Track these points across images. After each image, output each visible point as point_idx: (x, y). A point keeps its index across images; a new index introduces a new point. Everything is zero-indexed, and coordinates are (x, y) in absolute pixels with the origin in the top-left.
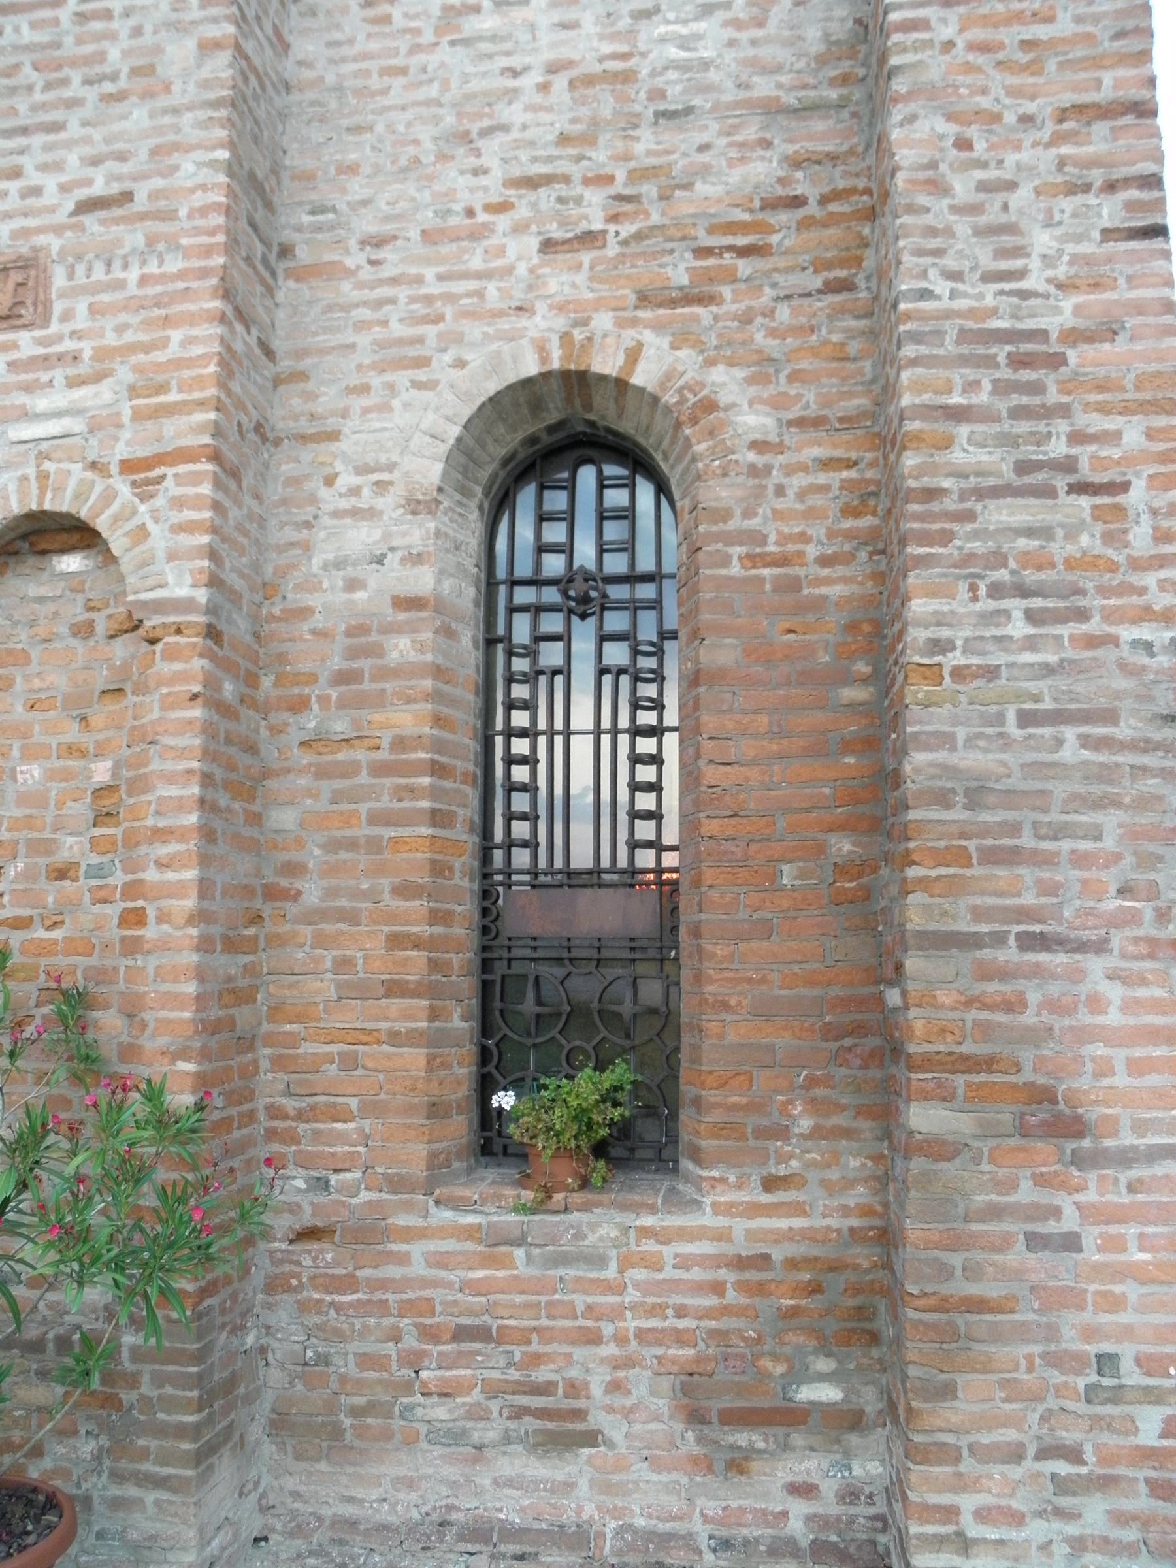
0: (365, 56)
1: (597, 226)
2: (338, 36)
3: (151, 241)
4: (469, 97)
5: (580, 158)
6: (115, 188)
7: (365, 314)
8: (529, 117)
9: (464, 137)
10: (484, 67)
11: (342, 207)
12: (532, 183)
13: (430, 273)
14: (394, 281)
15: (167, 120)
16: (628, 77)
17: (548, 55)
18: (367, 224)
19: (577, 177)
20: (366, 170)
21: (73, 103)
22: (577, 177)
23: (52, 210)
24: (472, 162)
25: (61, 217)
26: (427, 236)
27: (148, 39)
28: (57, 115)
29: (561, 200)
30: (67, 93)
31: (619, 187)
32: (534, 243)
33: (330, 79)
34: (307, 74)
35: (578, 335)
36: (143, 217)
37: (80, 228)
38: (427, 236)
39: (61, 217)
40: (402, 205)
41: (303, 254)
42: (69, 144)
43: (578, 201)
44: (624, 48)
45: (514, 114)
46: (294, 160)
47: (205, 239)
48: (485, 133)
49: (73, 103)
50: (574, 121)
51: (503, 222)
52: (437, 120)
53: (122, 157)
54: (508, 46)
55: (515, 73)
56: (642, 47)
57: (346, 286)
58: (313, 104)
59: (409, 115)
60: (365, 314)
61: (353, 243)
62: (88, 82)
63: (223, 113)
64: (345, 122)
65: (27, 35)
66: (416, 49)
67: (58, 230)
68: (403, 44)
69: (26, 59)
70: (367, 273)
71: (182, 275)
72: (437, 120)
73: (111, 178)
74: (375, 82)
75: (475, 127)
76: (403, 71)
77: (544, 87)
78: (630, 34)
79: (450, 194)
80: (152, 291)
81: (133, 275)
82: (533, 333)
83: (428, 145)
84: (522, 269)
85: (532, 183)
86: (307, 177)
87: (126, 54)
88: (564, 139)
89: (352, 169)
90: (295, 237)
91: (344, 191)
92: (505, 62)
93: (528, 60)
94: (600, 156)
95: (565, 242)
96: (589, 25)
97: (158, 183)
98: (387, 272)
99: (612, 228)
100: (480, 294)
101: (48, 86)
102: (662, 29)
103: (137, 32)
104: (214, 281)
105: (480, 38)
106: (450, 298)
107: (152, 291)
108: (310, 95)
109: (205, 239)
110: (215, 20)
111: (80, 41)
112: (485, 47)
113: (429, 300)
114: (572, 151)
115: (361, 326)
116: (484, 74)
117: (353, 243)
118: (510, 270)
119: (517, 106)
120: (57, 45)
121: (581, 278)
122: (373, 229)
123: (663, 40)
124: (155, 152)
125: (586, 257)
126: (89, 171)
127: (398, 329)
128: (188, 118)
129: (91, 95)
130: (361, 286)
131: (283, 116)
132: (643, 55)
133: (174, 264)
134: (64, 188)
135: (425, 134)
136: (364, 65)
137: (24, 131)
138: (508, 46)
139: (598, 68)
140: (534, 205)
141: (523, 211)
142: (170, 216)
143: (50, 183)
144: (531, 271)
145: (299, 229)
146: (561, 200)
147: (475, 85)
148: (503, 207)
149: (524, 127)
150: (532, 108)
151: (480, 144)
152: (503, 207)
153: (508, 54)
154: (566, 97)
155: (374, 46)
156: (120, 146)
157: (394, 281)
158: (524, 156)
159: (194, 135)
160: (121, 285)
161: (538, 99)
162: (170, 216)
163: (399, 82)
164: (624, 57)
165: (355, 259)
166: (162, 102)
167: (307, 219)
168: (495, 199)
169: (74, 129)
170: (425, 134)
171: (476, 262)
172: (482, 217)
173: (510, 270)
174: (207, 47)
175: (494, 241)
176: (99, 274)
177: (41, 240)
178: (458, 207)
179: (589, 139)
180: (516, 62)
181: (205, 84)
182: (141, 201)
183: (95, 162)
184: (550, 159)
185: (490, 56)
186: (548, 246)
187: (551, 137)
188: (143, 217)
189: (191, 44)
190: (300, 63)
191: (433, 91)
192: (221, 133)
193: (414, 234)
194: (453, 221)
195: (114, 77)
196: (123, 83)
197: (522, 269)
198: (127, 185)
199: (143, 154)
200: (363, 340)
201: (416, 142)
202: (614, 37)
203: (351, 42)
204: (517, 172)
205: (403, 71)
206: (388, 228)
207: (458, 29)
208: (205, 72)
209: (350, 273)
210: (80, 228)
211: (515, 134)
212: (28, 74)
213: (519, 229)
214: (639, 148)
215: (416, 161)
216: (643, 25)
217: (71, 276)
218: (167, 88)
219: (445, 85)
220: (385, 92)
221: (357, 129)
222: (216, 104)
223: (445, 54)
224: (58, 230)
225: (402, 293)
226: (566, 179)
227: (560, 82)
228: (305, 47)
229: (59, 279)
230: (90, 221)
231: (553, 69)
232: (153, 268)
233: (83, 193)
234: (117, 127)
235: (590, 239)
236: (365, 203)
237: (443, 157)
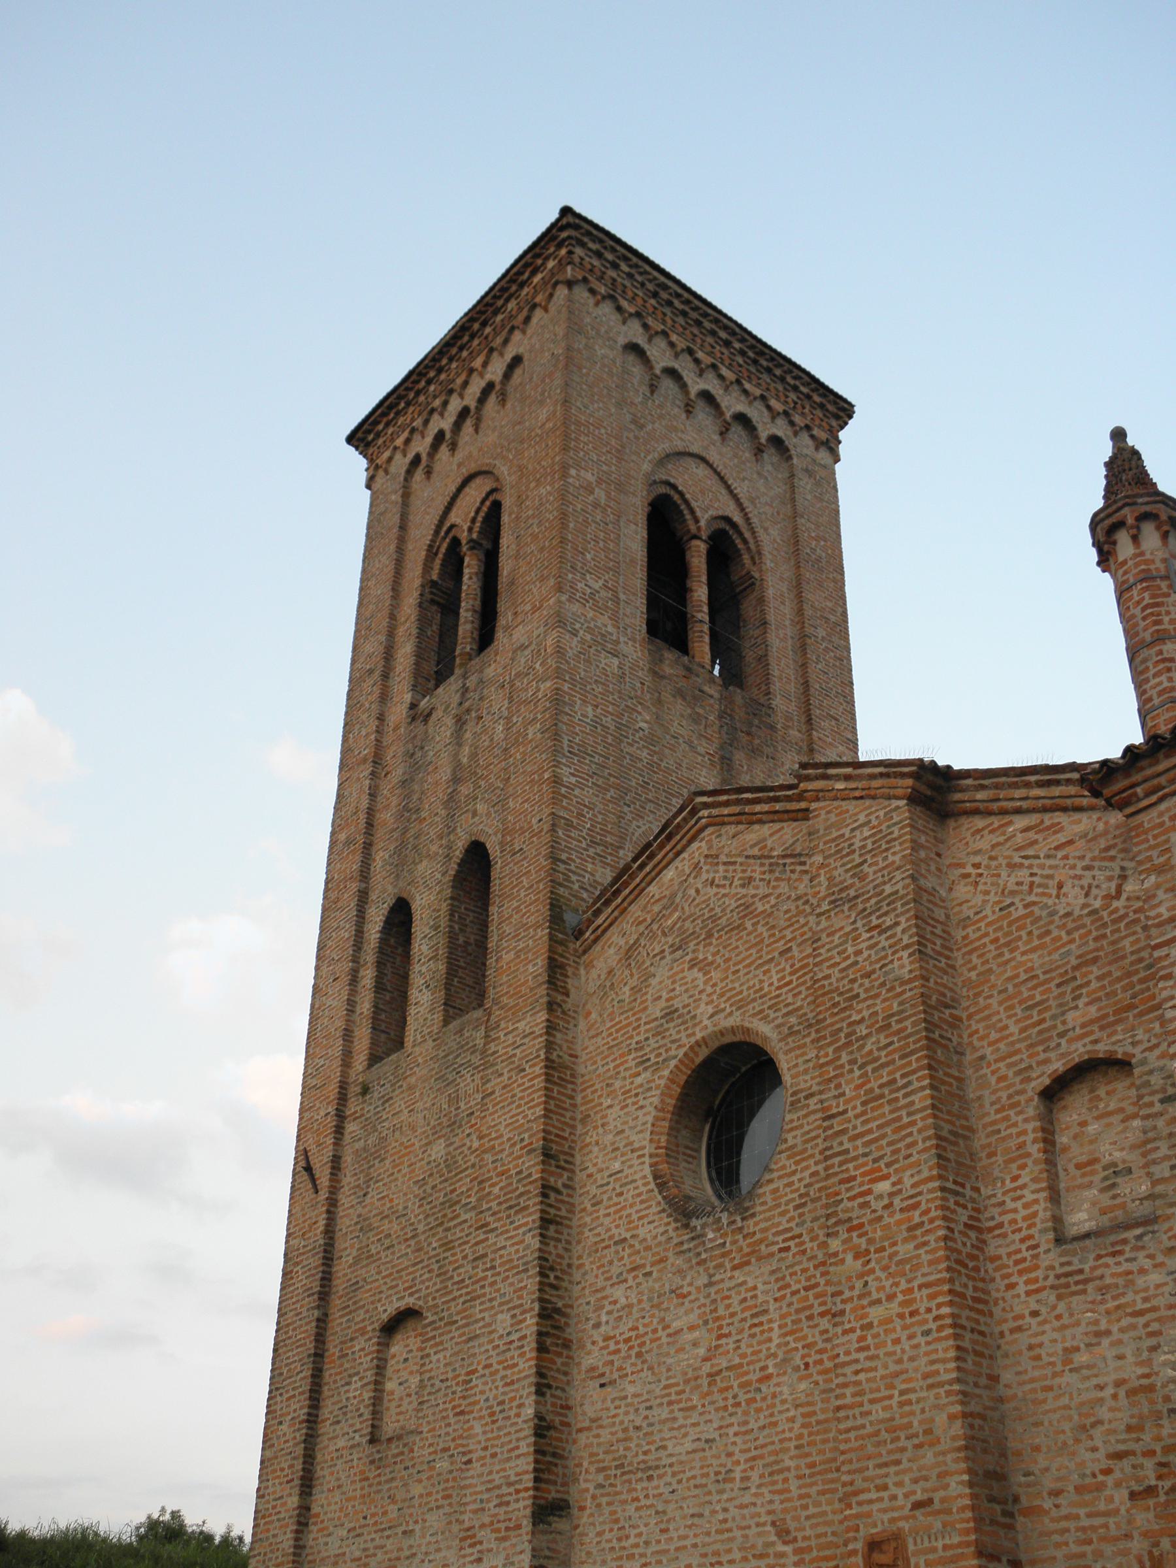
0: (1032, 1380)
1: (1153, 1483)
2: (1020, 1369)
3: (944, 1525)
4: (1082, 1404)
5: (1138, 1440)
6: (925, 1496)
7: (1056, 1538)
8: (1110, 1415)
9: (1083, 1428)
10: (1088, 1384)
11: (1037, 1472)
12: (1119, 1456)
13: (1082, 1512)
14: (1067, 1517)
15: (941, 1458)
16: (1151, 1388)
17: (1114, 1376)
18: (1048, 1483)
19: (1138, 1452)
20: (1044, 1449)
21: (903, 1450)
22: (1138, 1452)
23: (902, 1508)
24: (1090, 1444)
25: (906, 1512)
26: (1079, 1489)
27: (927, 1415)
28: (896, 1456)
29: (1134, 1467)
30: (900, 1444)
31: (1160, 1458)
32: (1125, 1493)
33: (1020, 1394)
34: (1010, 1392)
35: (1156, 1553)
36: (939, 1512)
37: (914, 1517)
38: (1079, 1489)
39: (906, 1512)
40: (1064, 1472)
41: (1025, 1502)
42: (904, 1472)
43: (1142, 1466)
44: (1146, 1370)
45: (1103, 1413)
46: (1012, 1444)
47: (965, 1525)
48: (1093, 1425)
49: (903, 1450)
50: (1132, 1417)
51: (1109, 1480)
52: (1070, 1418)
53: (926, 1479)
54: (1095, 1371)
55: (1101, 1388)
56: (1156, 1369)
57: (1046, 1520)
58: (1015, 1409)
59: (1057, 1416)
60: (1056, 1538)
61: (1045, 1494)
62: (907, 1438)
63: (962, 1455)
64: (1031, 1420)
65: (883, 1415)
66: (1055, 1375)
67: (906, 1518)
68: (1048, 1371)
69: (882, 1426)
70: (1054, 1513)
71: (959, 1545)
72: (1070, 1418)
73: (924, 1490)
74: (1040, 1396)
75: (1088, 1422)
76: (1051, 1388)
77: (1115, 1396)
78: (1148, 1362)
79: (1082, 1464)
80: (949, 1553)
81: (940, 1544)
82: (1135, 1552)
83: (1069, 1434)
84: (1123, 1511)
85: (1119, 1456)
86: (1018, 1453)
87: (920, 1422)
88: (1129, 1429)
89: (1037, 1449)
90: (1020, 1490)
91: (1036, 1462)
92: (1095, 1381)
93: (1106, 1379)
94: (1147, 1437)
95: (1140, 1493)
96: (1130, 1359)
97: (942, 1493)
98: (1064, 1511)
99: (1160, 1483)
100: (1106, 1526)
101: (892, 1441)
102: (1163, 1358)
103: (923, 1411)
104: (972, 1549)
105: (1081, 1367)
106: (1093, 1528)
107: (949, 1553)
108: (1012, 1404)
109: (965, 1525)
110: (952, 1404)
111: (902, 1417)
112: (1084, 1372)
113: (1084, 1529)
114: (1134, 1435)
115: (1058, 1545)
116: (1087, 1389)
117: (1045, 1494)
118: (1117, 1511)
119: (1105, 1409)
120: (892, 1419)
121: (1151, 1515)
122: (1053, 1486)
123: (1165, 1364)
124: (939, 1476)
125: (1151, 1502)
126: (914, 1487)
127: (1074, 1549)
128: (949, 1457)
129: (909, 1444)
130: (1053, 1520)
131: (1002, 1421)
132: (1157, 1374)
133: (956, 1539)
134: (906, 1496)
135: (1067, 1426)
136: (1033, 1385)
137: (886, 1465)
138: (1095, 1371)
139: (1137, 1383)
140: (1122, 1470)
141: (1117, 1474)
142: (949, 1512)
143: (900, 1492)
144: (1128, 1511)
145: (1020, 1485)
146: (1134, 1467)
147: (1085, 1396)
148: (1107, 1472)
149: (1110, 1422)
150: (1111, 1409)
151: (1092, 1432)
152: (1107, 1472)
153: (1096, 1376)
154: (1126, 1402)
155: (1037, 1373)
156: (924, 1473)
157: (1067, 1517)
158: (1112, 1439)
159: (953, 1467)
160: (934, 1550)
161: (1113, 1403)
162: (949, 1512)
163: (1050, 1395)
164: (1147, 1376)
165: (1047, 1504)
166: (938, 1448)
167: (1023, 1479)
168: (1104, 1467)
169: (905, 1464)
170: (1067, 1426)
171: (1102, 1506)
172: (1101, 1478)
173: (1117, 1511)
174: (952, 1417)
175: (1108, 1492)
176: (926, 1544)
177: (901, 1524)
178: (1088, 1472)
179: (1140, 1428)
180: (1100, 1380)
181: (954, 1438)
182: (937, 1505)
183: (915, 1481)
184: (1124, 1441)
185: (1088, 1378)
186: (1133, 1495)
187: (1123, 1427)
188: (939, 1512)
189: (945, 1416)
190: (1006, 1386)
191: (1065, 1400)
192: (963, 1465)
193: (1071, 1489)
194: (1088, 1480)
195: (916, 1435)
196: (921, 1439)
197: (1123, 1511)
198: (931, 1495)
199: (934, 1477)
200: (1059, 1554)
201: (1063, 1432)
202: (1141, 1364)
203: (1026, 1371)
204: (1111, 1450)
205: (1051, 1388)
206: (1059, 1485)
207: (1071, 1362)
208: (952, 1432)
209: (1047, 1512)
210: (914, 1517)
211: (1106, 1426)
212: (884, 1435)
213: (1118, 1485)
214: (1165, 1432)
215: (1065, 1443)
216: (1154, 1355)
217: (915, 1543)
218: (938, 1441)
219: (1071, 1398)
220: (1044, 1401)
221: (1036, 1424)
222: (959, 1449)
223: (1068, 1378)
224: (906, 1518)
225: (1072, 1525)
226: (1133, 1453)
227: (1122, 1393)
228: (1007, 1377)
229: (911, 1547)
230: (917, 1513)
231: (1119, 1384)
232: (947, 1541)
233: (913, 1498)
234: (922, 1462)
235: (1151, 1491)
236: (1047, 1469)
237: (1077, 1441)
